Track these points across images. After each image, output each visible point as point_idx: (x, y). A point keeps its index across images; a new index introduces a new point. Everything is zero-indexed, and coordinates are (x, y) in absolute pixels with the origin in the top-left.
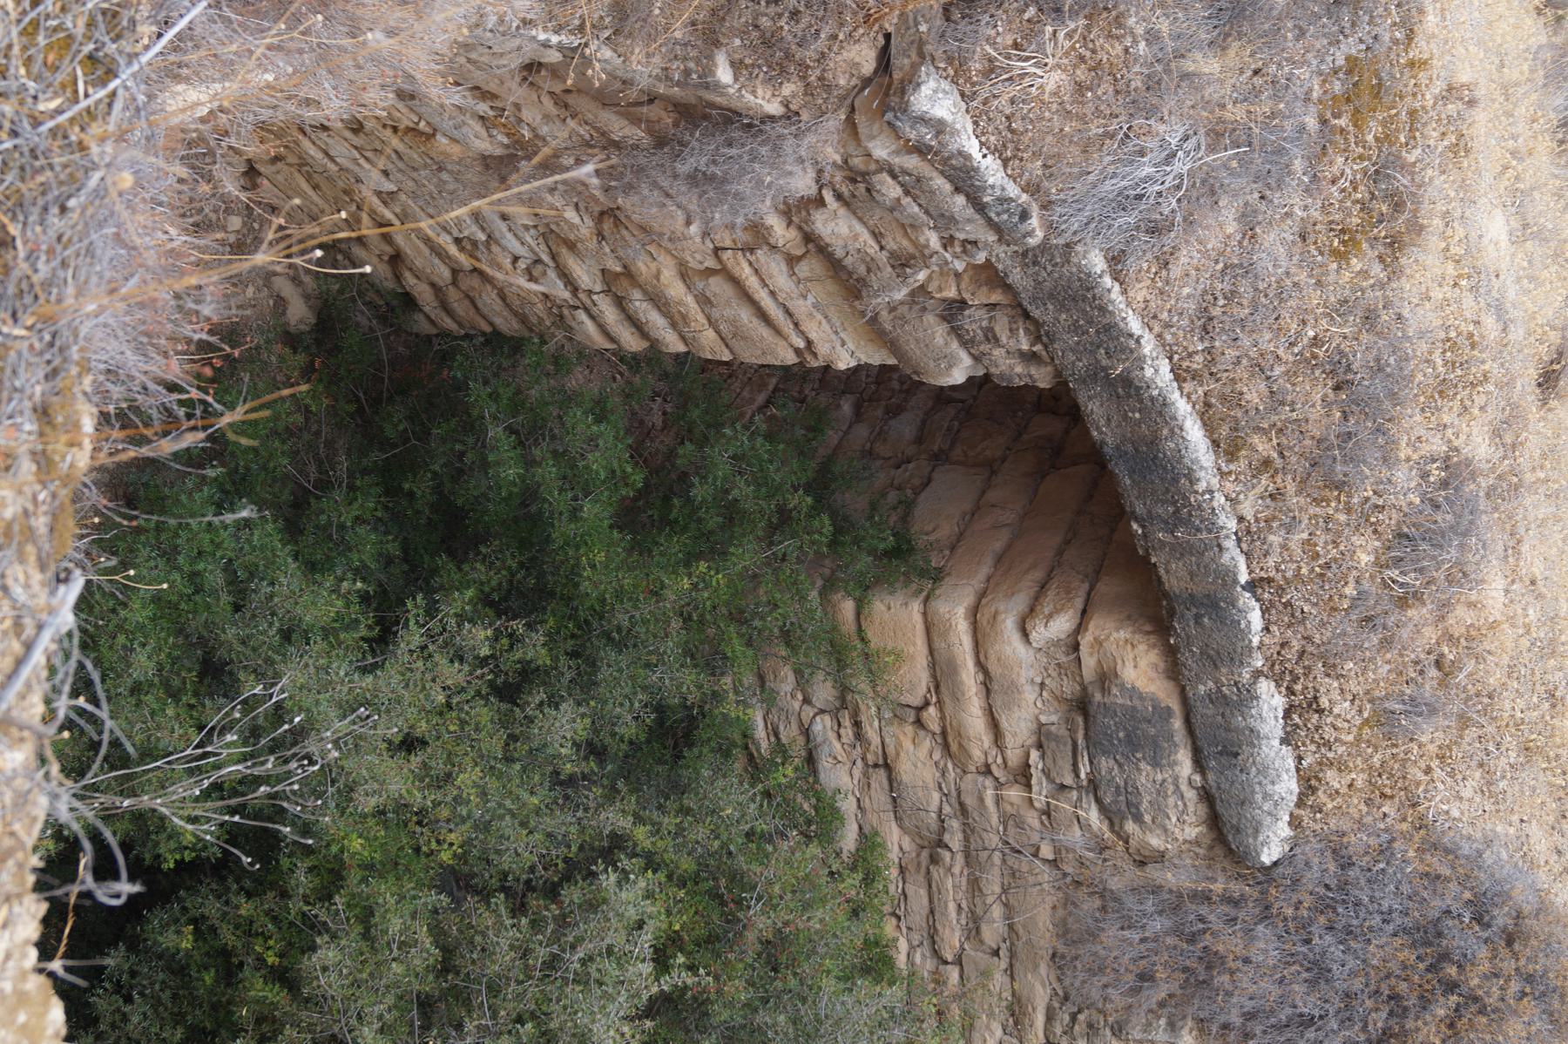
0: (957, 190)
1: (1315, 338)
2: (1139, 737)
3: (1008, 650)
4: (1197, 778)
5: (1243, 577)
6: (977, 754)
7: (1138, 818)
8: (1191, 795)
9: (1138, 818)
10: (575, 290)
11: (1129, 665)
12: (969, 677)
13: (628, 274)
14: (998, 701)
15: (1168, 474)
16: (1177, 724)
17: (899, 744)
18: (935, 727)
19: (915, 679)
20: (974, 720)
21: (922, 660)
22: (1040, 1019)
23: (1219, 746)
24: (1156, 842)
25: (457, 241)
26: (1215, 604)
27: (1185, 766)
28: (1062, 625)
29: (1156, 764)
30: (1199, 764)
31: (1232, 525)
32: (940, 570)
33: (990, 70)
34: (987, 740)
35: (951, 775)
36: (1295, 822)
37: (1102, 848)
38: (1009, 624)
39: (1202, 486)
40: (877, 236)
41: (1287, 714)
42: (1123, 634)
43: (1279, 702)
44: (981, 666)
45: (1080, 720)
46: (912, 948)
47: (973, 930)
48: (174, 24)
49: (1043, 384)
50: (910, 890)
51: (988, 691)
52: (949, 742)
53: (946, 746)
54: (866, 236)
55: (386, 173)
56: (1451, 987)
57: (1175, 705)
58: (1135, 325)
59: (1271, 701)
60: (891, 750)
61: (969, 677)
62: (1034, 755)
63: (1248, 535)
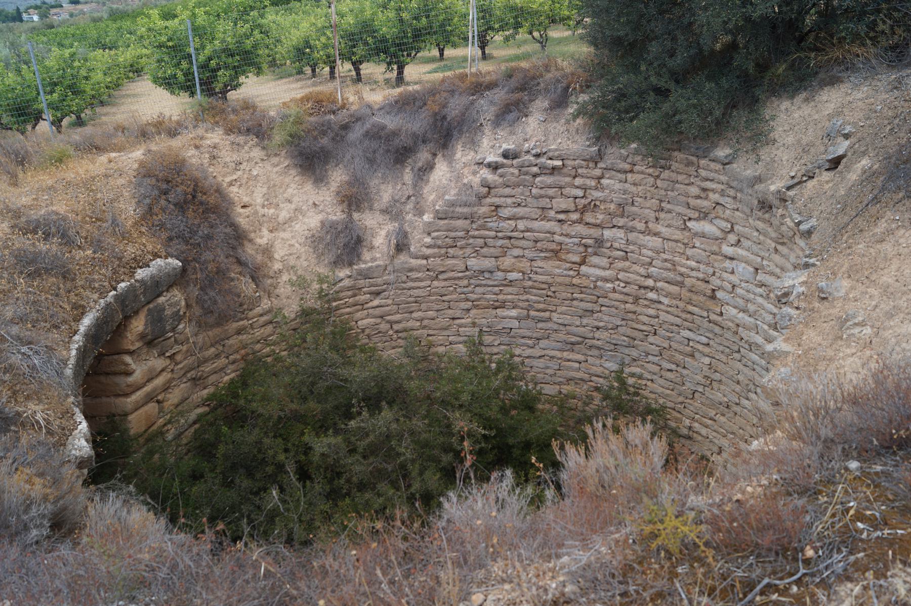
1: (758, 65)
2: (157, 318)
3: (140, 376)
4: (165, 294)
5: (113, 293)
9: (179, 311)
11: (138, 329)
12: (148, 388)
14: (154, 374)
16: (151, 306)
19: (152, 407)
20: (159, 381)
21: (146, 408)
23: (156, 287)
24: (183, 303)
27: (161, 300)
29: (164, 309)
32: (108, 417)
33: (50, 433)
34: (164, 374)
35: (174, 383)
36: (166, 258)
37: (190, 320)
38: (131, 379)
41: (141, 268)
42: (129, 335)
43: (139, 271)
44: (144, 385)
45: (156, 341)
46: (227, 374)
47: (217, 356)
50: (210, 382)
51: (152, 379)
52: (166, 388)
53: (168, 388)
56: (194, 197)
57: (146, 308)
58: (74, 352)
59: (141, 274)
61: (148, 388)
63: (103, 295)
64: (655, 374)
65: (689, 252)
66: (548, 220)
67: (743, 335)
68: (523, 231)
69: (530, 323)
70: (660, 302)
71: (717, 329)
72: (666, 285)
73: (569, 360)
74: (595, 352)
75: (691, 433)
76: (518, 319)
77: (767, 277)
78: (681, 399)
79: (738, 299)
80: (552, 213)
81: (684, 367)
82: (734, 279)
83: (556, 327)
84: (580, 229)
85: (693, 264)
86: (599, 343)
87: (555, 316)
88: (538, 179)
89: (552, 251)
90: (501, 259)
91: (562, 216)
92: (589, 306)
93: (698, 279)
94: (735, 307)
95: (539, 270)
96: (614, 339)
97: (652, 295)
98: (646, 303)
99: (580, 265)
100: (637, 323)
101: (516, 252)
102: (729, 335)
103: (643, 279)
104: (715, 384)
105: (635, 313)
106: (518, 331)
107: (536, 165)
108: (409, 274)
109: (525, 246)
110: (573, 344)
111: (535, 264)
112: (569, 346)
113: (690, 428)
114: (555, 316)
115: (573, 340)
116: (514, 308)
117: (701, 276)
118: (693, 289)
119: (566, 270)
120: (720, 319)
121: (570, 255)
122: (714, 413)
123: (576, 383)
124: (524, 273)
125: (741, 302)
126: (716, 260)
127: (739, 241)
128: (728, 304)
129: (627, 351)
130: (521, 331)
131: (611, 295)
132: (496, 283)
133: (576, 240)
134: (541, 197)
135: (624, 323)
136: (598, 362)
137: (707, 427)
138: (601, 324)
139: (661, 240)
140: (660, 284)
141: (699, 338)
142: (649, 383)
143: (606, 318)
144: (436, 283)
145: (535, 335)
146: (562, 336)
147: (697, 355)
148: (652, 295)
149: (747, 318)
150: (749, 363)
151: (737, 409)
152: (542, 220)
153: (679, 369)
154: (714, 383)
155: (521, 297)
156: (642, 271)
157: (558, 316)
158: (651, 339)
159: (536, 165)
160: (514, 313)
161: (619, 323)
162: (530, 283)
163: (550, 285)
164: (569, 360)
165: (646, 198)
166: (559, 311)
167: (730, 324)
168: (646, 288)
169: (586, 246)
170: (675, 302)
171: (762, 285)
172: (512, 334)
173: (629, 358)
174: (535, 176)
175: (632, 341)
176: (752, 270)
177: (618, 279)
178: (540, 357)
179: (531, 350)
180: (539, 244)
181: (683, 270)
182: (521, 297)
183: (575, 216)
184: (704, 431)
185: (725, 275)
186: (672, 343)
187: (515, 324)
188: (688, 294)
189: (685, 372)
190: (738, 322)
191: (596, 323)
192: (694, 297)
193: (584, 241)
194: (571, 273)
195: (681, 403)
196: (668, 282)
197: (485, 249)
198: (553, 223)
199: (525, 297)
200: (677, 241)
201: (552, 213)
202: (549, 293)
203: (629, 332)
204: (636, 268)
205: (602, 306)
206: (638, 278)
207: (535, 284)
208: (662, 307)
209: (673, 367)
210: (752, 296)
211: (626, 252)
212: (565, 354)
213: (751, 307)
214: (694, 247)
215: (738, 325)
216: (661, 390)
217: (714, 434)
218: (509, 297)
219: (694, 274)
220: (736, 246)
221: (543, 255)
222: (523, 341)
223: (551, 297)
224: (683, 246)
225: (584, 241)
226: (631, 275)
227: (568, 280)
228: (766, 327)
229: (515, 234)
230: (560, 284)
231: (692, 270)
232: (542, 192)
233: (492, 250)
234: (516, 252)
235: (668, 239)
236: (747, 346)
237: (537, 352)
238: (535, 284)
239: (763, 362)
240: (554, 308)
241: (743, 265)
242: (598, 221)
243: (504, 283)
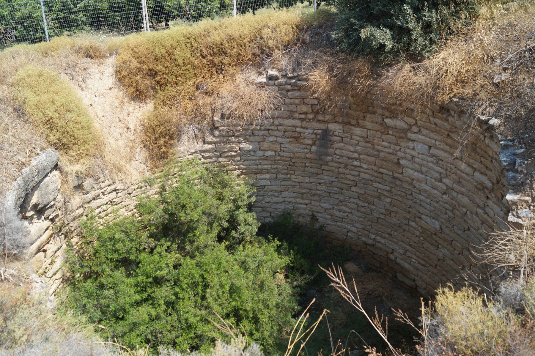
7: (57, 186)
9: (57, 186)
64: (354, 209)
65: (384, 137)
66: (293, 119)
67: (416, 185)
68: (277, 126)
69: (278, 182)
70: (361, 167)
71: (398, 182)
72: (366, 156)
73: (300, 204)
74: (317, 198)
75: (374, 242)
76: (270, 180)
77: (438, 151)
78: (369, 223)
79: (415, 164)
80: (296, 115)
81: (373, 205)
82: (413, 152)
83: (293, 184)
84: (316, 125)
85: (386, 144)
86: (320, 192)
87: (293, 177)
88: (290, 93)
89: (294, 137)
90: (261, 143)
91: (303, 116)
92: (315, 170)
93: (389, 153)
94: (412, 169)
95: (285, 149)
96: (329, 190)
97: (356, 163)
98: (352, 168)
99: (312, 146)
100: (345, 180)
101: (272, 139)
102: (406, 186)
103: (351, 153)
104: (393, 215)
105: (344, 174)
106: (269, 187)
107: (290, 84)
108: (203, 154)
109: (278, 135)
110: (303, 194)
111: (283, 146)
112: (300, 195)
113: (374, 239)
114: (293, 177)
115: (304, 191)
116: (267, 173)
117: (391, 151)
118: (385, 159)
119: (302, 149)
120: (401, 176)
121: (306, 140)
122: (390, 230)
123: (303, 217)
124: (275, 152)
125: (417, 167)
126: (402, 142)
127: (420, 130)
128: (407, 167)
129: (337, 196)
130: (271, 187)
131: (330, 164)
132: (258, 158)
133: (310, 131)
134: (291, 104)
135: (336, 180)
136: (318, 204)
137: (385, 238)
138: (322, 181)
139: (366, 130)
140: (362, 156)
141: (384, 187)
142: (349, 215)
143: (325, 177)
144: (220, 160)
145: (279, 189)
146: (296, 190)
147: (382, 197)
148: (356, 163)
149: (420, 175)
150: (418, 201)
151: (406, 227)
152: (289, 118)
153: (370, 206)
154: (392, 213)
155: (273, 166)
156: (352, 149)
157: (295, 177)
158: (353, 189)
159: (290, 84)
160: (268, 176)
161: (333, 180)
162: (279, 158)
163: (291, 158)
164: (300, 204)
165: (359, 105)
166: (296, 174)
167: (408, 179)
168: (352, 158)
169: (316, 134)
170: (371, 167)
171: (433, 156)
172: (266, 189)
173: (338, 201)
174: (288, 91)
175: (340, 190)
176: (427, 147)
177: (335, 154)
178: (282, 202)
179: (276, 199)
180: (286, 134)
181: (379, 148)
182: (273, 166)
183: (311, 116)
184: (383, 241)
185: (408, 151)
186: (366, 191)
187: (268, 183)
188: (381, 162)
189: (373, 207)
190: (413, 177)
191: (319, 181)
192: (385, 163)
193: (315, 131)
194: (306, 150)
195: (370, 225)
196: (368, 155)
197: (252, 137)
198: (296, 121)
199: (275, 166)
200: (376, 131)
201: (296, 115)
202: (291, 163)
203: (339, 185)
204: (347, 147)
205: (323, 170)
206: (349, 153)
207: (282, 158)
208: (362, 170)
209: (366, 205)
210: (426, 162)
211: (342, 137)
212: (298, 200)
213: (424, 169)
214: (388, 134)
215: (413, 179)
216: (356, 218)
217: (390, 242)
218: (265, 166)
219: (387, 150)
220: (417, 133)
221: (288, 140)
222: (272, 193)
223: (292, 166)
224: (380, 134)
225: (315, 131)
226: (344, 151)
227: (303, 155)
228: (433, 180)
229: (272, 127)
230: (298, 158)
231: (385, 147)
232: (292, 101)
233: (257, 137)
234: (272, 139)
235: (370, 130)
236: (418, 192)
237: (280, 199)
238: (282, 158)
239: (428, 201)
240: (293, 172)
241: (421, 144)
242: (326, 119)
243: (263, 158)
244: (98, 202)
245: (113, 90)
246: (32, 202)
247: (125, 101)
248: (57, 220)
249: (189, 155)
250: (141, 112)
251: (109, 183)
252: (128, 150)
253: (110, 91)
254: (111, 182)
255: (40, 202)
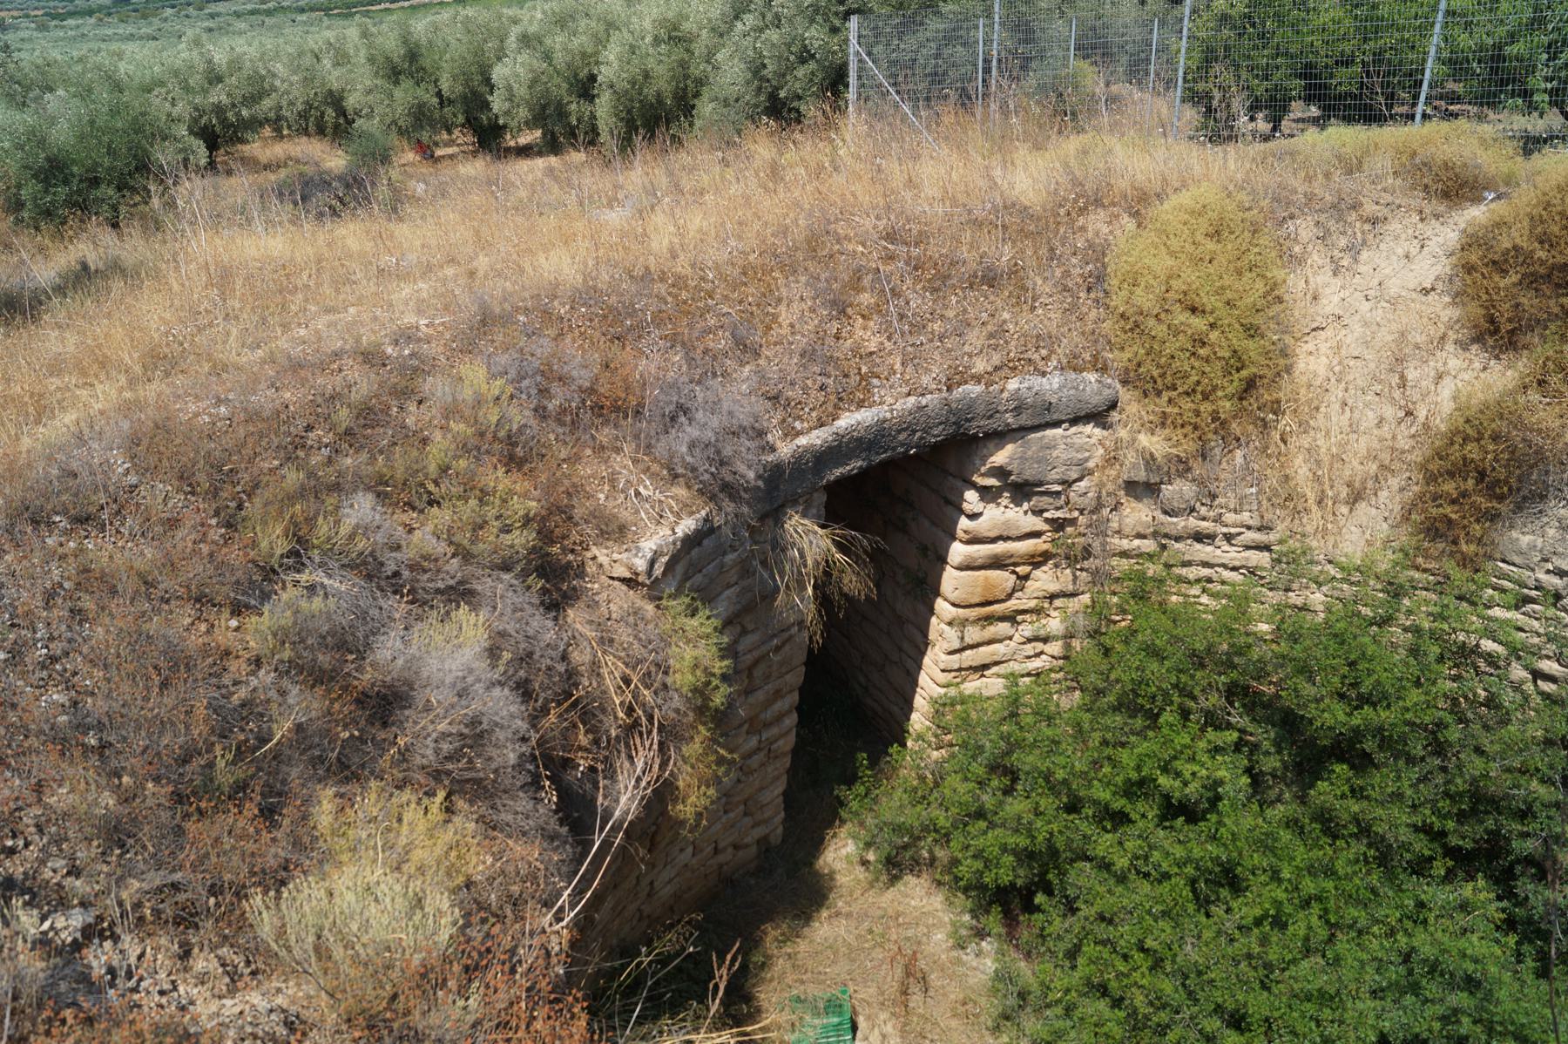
0: (699, 544)
6: (1046, 547)
7: (1087, 460)
8: (1073, 430)
9: (1087, 460)
10: (759, 749)
12: (1000, 547)
13: (751, 720)
15: (875, 439)
17: (1038, 589)
18: (1028, 569)
22: (1204, 524)
25: (726, 812)
26: (958, 416)
28: (971, 496)
30: (1056, 424)
31: (912, 399)
39: (888, 415)
40: (729, 586)
44: (993, 540)
48: (1422, 81)
49: (825, 498)
54: (727, 592)
55: (682, 850)
60: (1041, 594)
61: (1000, 547)
62: (1046, 515)
244: (1203, 551)
245: (1432, 296)
246: (992, 459)
247: (1452, 336)
248: (1069, 530)
249: (1548, 572)
250: (1465, 381)
251: (1251, 522)
252: (1373, 467)
253: (1424, 299)
254: (1255, 522)
255: (1013, 467)
